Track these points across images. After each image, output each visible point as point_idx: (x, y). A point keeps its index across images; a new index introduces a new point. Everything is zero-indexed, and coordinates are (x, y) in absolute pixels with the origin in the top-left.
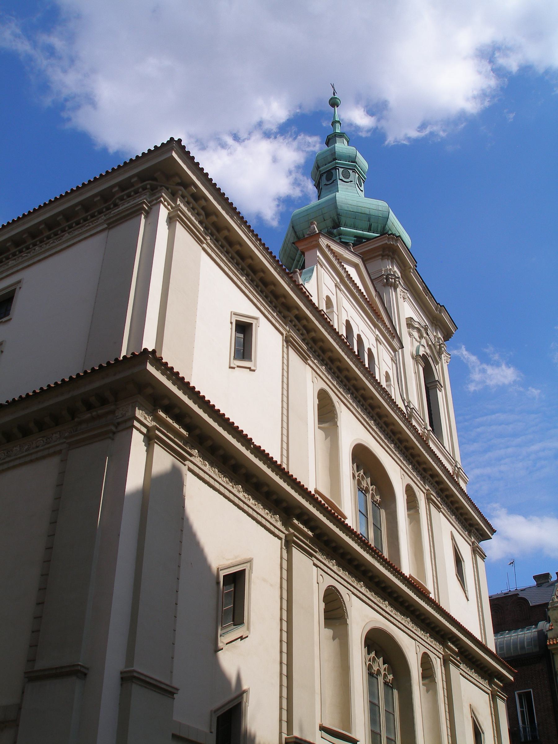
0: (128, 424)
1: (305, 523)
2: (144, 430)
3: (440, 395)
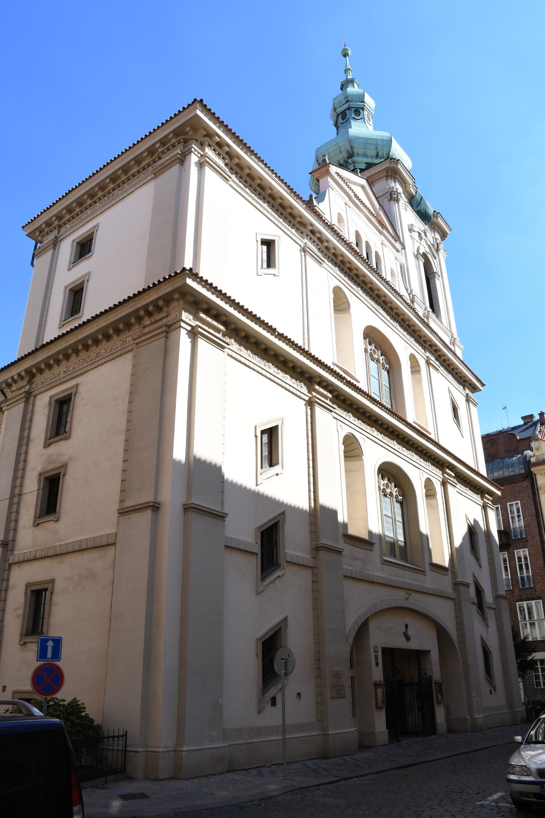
0: (177, 325)
1: (325, 388)
2: (189, 328)
3: (438, 283)
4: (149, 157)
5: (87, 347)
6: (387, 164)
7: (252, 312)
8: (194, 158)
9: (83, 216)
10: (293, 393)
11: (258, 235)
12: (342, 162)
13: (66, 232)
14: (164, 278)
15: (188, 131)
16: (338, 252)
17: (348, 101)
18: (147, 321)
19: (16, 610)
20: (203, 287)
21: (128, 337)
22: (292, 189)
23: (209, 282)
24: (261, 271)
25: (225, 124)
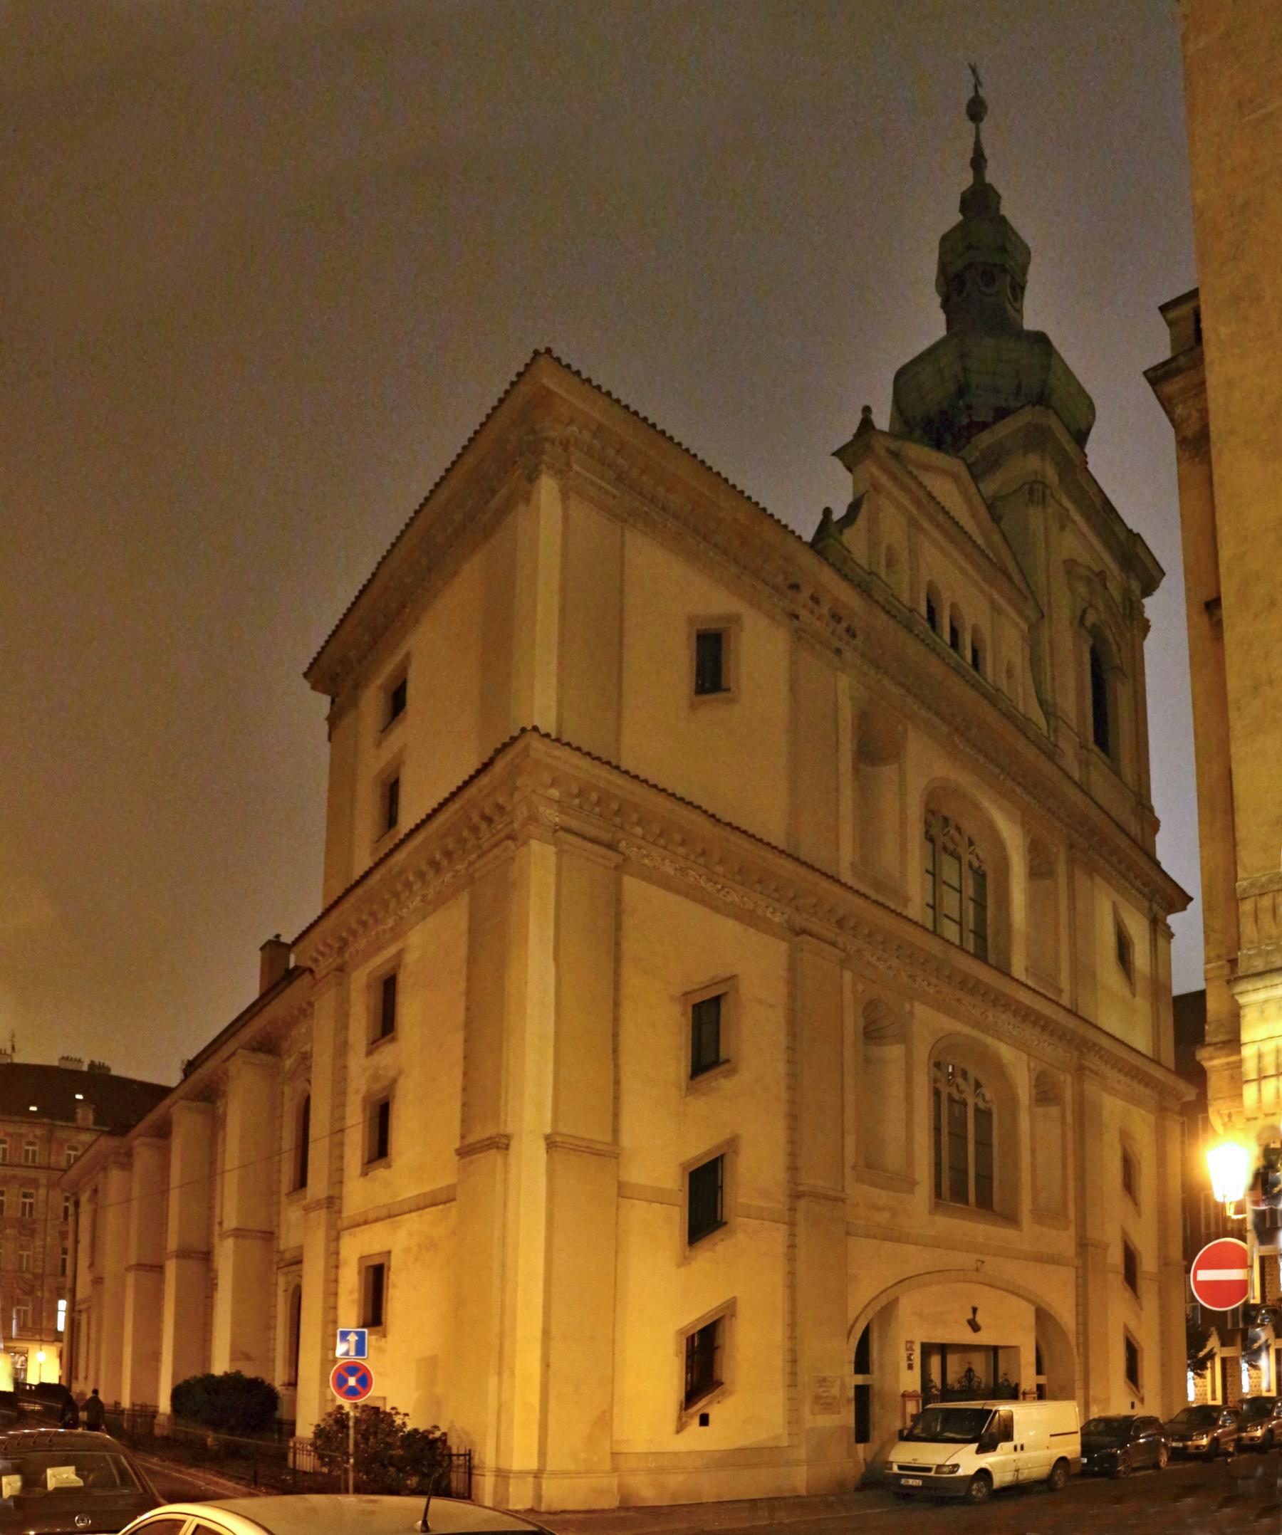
17: (969, 247)
19: (351, 1293)
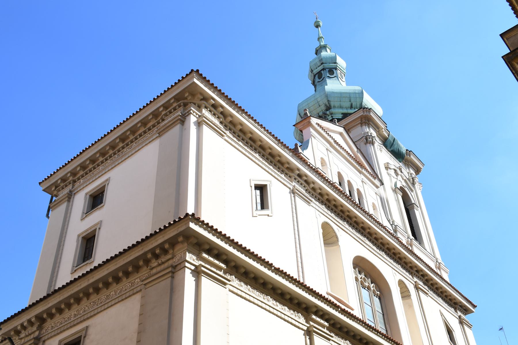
0: (182, 265)
1: (321, 317)
2: (193, 268)
3: (418, 213)
4: (154, 119)
5: (97, 290)
6: (361, 113)
7: (249, 250)
8: (193, 119)
9: (95, 172)
10: (291, 324)
11: (252, 181)
12: (321, 114)
13: (80, 186)
14: (170, 223)
15: (187, 96)
16: (323, 192)
17: (322, 64)
18: (154, 263)
20: (205, 229)
21: (136, 279)
22: (280, 140)
23: (210, 225)
24: (256, 213)
25: (218, 89)
